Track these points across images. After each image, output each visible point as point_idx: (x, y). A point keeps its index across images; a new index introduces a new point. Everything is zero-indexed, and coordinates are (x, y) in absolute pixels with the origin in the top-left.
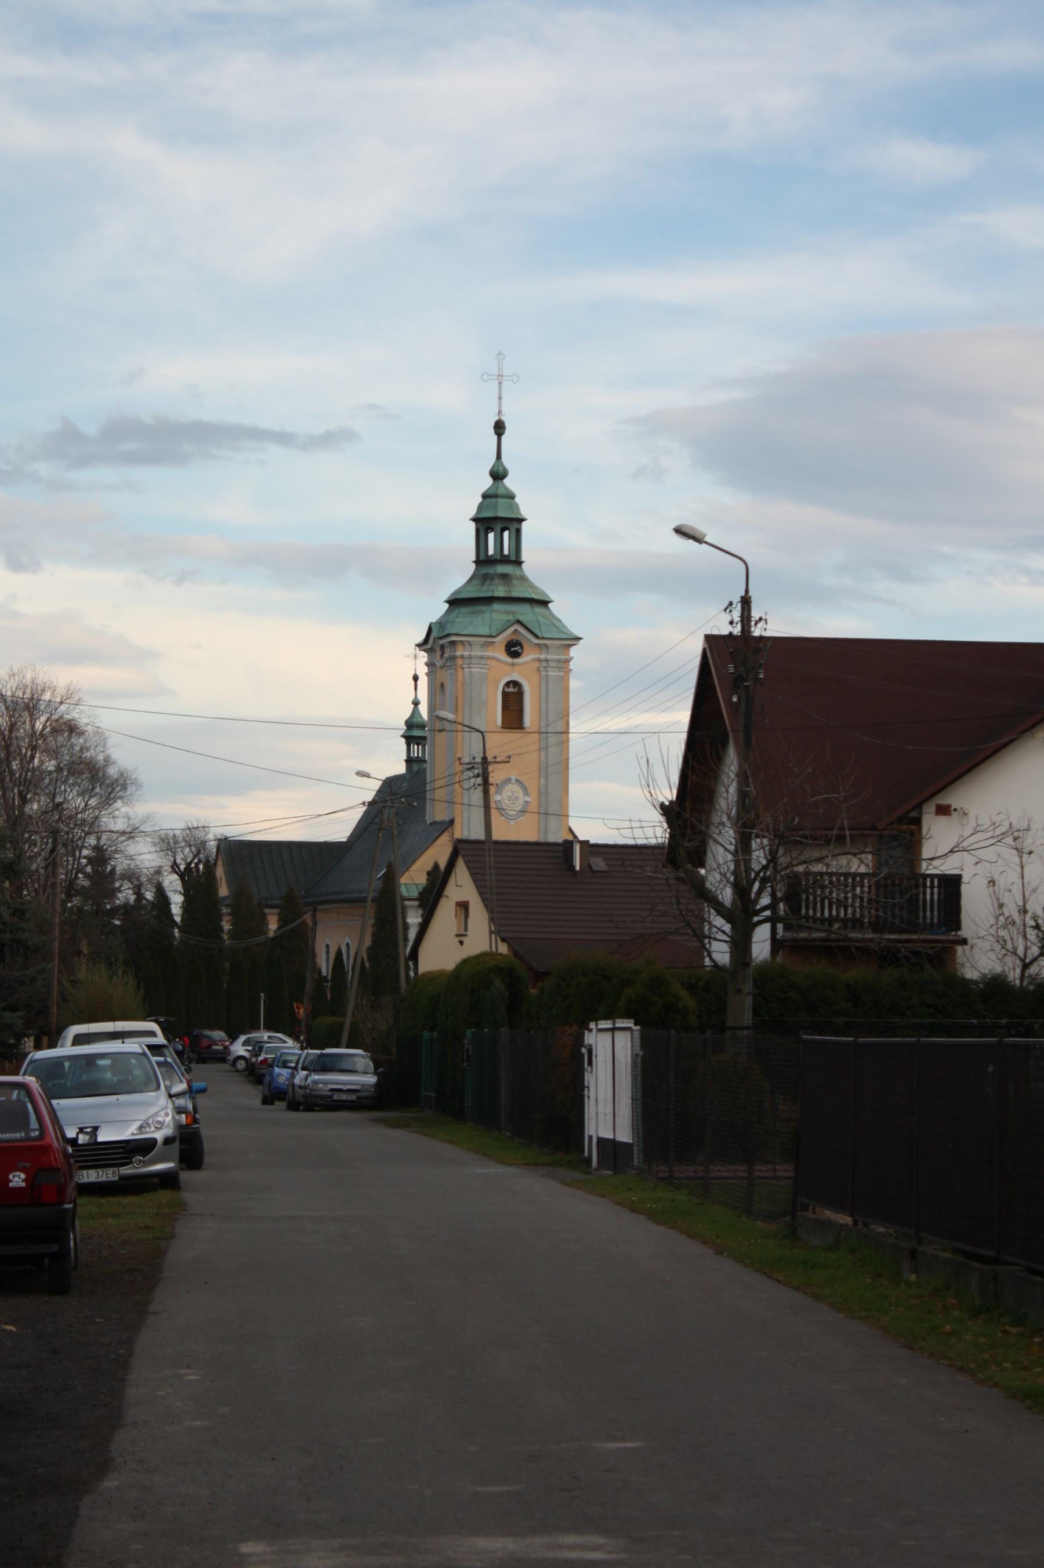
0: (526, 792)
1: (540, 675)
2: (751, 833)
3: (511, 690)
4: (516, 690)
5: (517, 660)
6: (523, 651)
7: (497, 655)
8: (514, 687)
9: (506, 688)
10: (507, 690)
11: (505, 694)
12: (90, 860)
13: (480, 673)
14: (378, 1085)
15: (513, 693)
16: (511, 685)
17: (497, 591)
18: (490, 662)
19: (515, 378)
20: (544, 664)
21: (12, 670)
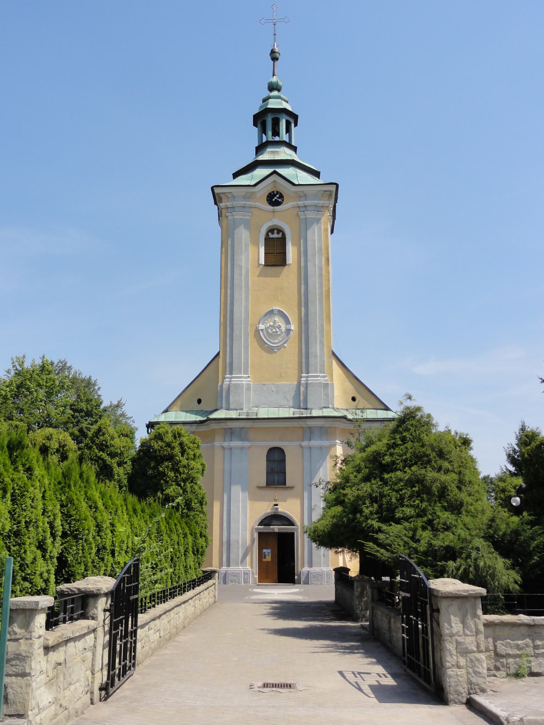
0: (288, 322)
1: (300, 219)
2: (518, 456)
3: (275, 236)
4: (280, 236)
5: (276, 208)
6: (283, 200)
7: (258, 204)
8: (278, 233)
9: (270, 234)
10: (271, 236)
11: (267, 240)
12: (92, 447)
13: (241, 219)
14: (369, 624)
15: (278, 238)
16: (276, 231)
17: (493, 663)
18: (252, 210)
19: (286, 20)
20: (303, 209)
21: (351, 558)
